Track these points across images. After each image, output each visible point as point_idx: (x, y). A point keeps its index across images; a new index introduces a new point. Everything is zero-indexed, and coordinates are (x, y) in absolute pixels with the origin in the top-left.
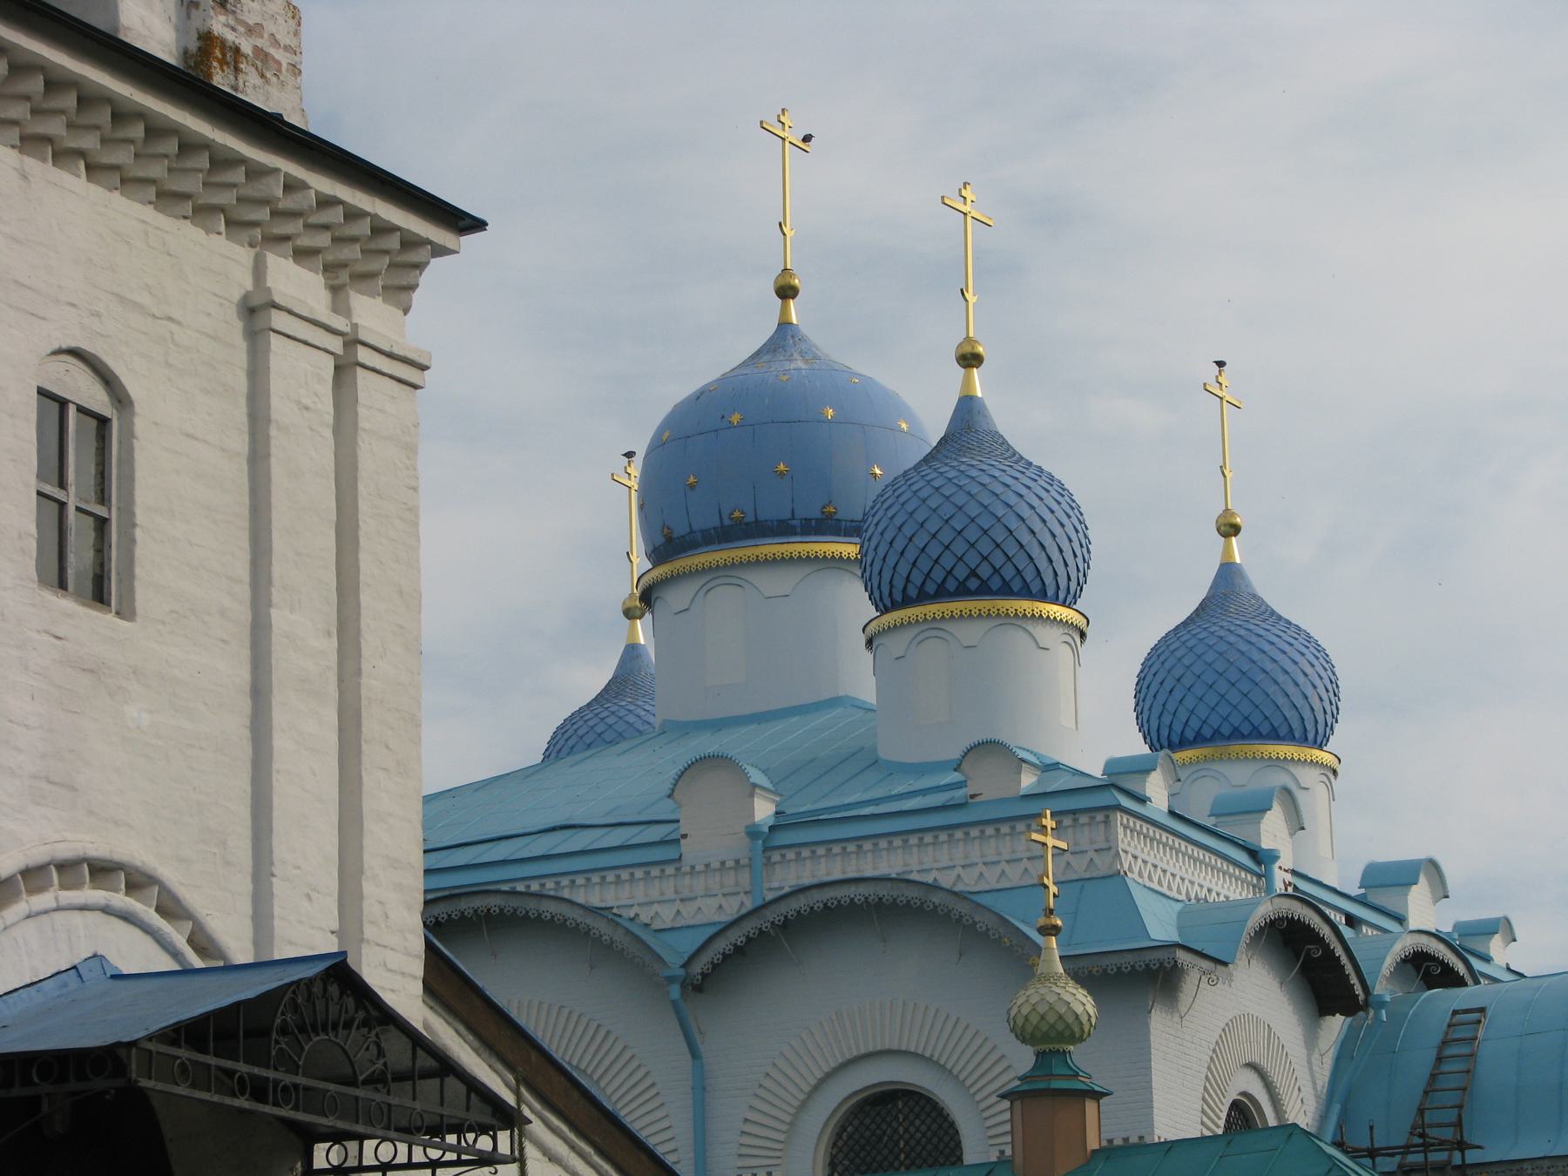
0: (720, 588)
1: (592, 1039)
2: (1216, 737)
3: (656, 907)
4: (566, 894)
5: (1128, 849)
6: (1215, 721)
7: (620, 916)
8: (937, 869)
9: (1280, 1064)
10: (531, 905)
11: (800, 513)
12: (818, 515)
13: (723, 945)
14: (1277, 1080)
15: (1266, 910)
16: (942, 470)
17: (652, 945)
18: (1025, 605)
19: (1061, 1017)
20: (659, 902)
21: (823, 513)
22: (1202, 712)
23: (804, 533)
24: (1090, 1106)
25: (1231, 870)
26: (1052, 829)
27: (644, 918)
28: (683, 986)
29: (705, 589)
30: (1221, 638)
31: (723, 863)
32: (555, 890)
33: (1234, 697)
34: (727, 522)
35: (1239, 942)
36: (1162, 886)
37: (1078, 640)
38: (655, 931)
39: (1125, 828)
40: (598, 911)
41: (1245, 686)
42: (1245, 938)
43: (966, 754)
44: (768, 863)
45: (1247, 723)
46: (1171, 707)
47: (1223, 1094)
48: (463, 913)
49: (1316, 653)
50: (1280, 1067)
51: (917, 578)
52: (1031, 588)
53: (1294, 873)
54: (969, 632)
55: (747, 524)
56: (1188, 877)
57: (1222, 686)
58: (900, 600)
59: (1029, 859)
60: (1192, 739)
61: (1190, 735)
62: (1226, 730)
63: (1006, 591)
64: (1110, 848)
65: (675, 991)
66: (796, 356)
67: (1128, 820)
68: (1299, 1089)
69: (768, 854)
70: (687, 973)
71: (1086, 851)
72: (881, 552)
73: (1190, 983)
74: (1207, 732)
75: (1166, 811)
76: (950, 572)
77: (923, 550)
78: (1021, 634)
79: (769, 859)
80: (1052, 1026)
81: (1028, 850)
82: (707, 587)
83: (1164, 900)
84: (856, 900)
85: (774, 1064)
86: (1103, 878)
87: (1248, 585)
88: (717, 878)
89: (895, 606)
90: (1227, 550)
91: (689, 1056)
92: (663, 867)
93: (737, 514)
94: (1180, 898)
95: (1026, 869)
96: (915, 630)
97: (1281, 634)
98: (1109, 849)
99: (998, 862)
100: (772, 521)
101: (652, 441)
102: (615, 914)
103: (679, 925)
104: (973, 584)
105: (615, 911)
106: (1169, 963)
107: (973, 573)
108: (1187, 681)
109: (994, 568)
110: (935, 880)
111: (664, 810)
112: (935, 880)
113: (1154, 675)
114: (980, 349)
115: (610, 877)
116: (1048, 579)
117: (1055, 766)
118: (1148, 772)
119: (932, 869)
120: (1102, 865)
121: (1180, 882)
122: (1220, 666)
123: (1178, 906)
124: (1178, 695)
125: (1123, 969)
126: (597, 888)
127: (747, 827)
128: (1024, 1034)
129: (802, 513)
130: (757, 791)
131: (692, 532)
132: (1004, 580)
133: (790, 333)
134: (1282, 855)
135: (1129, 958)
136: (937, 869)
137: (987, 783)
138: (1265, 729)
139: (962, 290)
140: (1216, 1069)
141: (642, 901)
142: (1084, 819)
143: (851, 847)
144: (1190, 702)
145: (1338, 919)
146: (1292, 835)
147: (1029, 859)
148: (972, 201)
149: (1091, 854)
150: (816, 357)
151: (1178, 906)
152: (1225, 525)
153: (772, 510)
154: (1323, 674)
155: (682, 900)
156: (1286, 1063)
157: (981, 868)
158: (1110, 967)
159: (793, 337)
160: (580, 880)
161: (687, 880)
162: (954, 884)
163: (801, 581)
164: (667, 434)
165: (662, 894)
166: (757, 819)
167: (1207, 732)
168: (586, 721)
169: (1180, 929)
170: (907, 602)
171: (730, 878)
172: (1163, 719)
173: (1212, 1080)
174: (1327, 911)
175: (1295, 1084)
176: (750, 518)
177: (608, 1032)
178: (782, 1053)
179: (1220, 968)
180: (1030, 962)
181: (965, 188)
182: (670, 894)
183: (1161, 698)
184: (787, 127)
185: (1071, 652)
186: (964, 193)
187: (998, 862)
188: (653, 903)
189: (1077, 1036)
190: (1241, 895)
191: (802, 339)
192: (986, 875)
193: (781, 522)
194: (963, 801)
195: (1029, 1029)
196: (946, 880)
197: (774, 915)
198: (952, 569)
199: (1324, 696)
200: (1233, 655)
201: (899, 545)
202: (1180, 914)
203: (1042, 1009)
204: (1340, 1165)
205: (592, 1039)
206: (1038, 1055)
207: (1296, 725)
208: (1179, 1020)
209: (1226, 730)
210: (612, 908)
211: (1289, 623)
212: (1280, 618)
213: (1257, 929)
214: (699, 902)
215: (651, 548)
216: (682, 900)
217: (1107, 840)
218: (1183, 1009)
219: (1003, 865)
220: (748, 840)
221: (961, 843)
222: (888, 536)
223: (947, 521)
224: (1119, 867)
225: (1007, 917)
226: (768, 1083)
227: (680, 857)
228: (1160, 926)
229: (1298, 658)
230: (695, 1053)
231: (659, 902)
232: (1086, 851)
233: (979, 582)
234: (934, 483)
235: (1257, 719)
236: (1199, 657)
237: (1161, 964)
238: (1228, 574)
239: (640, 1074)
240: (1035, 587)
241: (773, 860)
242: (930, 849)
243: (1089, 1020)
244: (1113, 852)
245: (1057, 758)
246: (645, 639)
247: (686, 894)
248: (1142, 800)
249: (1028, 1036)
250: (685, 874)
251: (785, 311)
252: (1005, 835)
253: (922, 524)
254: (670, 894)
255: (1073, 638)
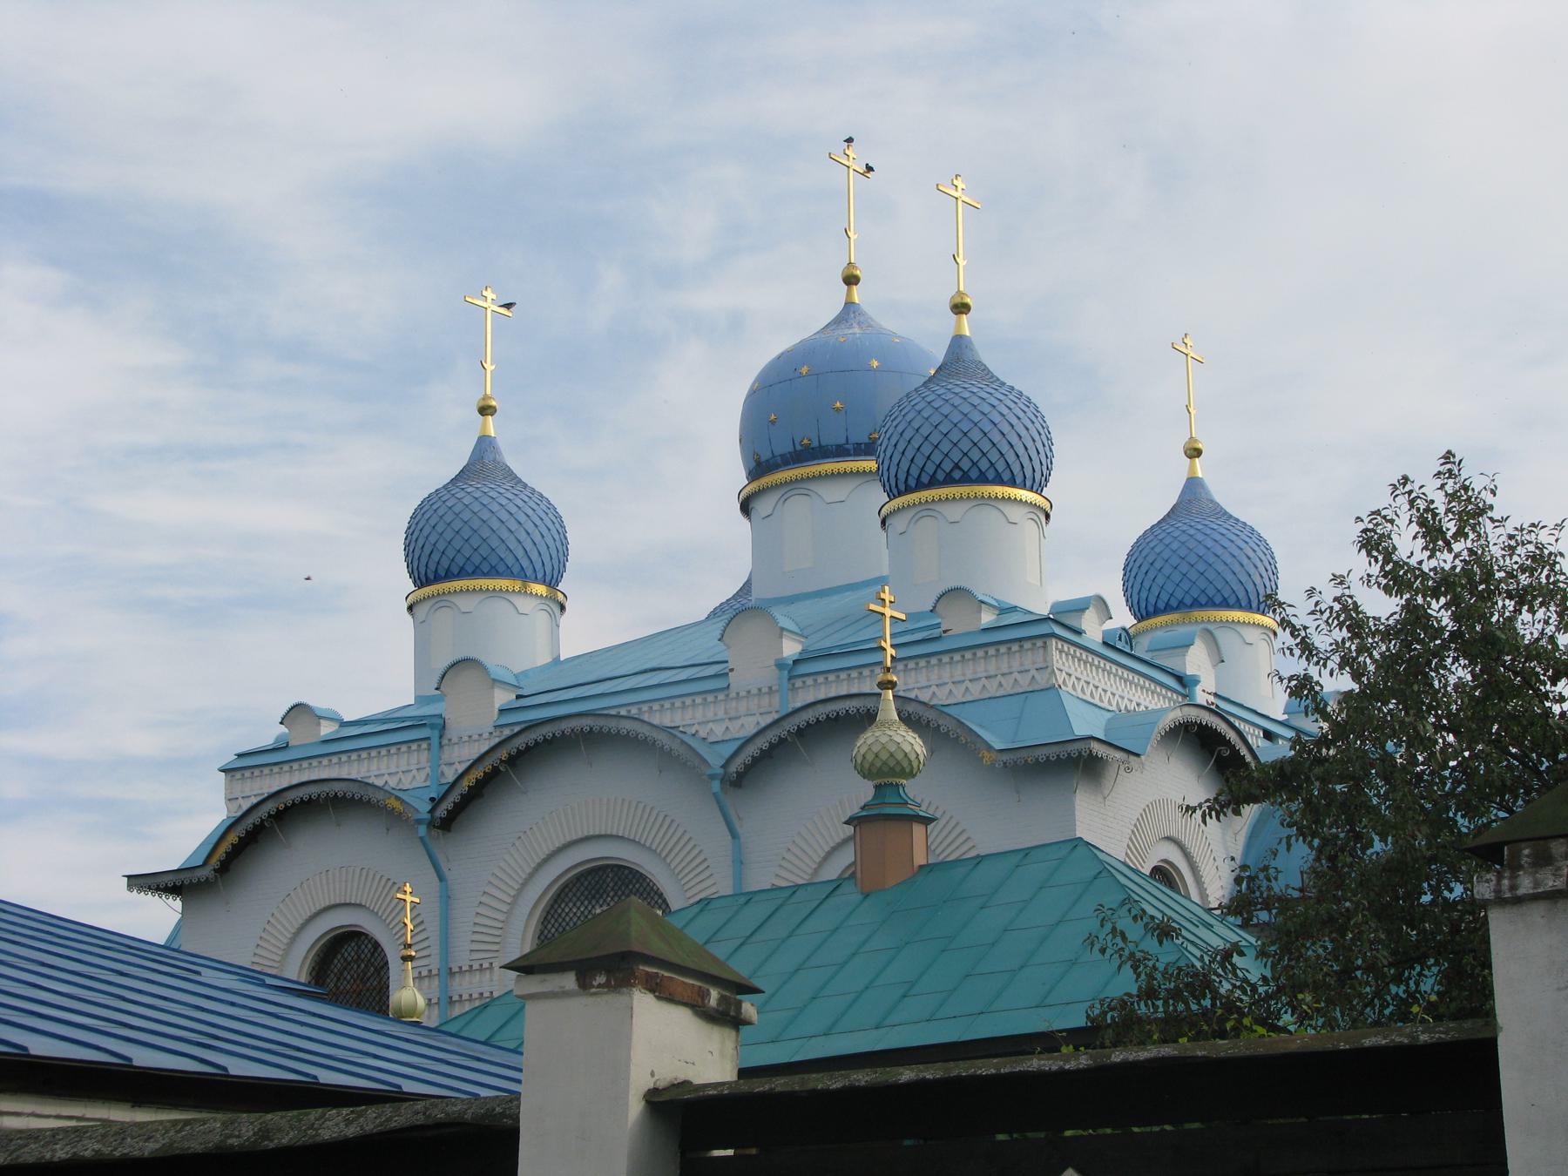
0: (797, 497)
1: (661, 826)
2: (1181, 606)
3: (711, 725)
4: (646, 717)
5: (1062, 668)
6: (1179, 595)
7: (685, 733)
8: (918, 688)
9: (1197, 839)
10: (612, 724)
11: (853, 439)
12: (867, 441)
13: (752, 750)
14: (1197, 855)
15: (1177, 715)
16: (939, 392)
17: (701, 753)
18: (999, 490)
19: (892, 755)
20: (713, 721)
21: (870, 438)
22: (1170, 588)
23: (855, 455)
24: (918, 830)
25: (1158, 690)
26: (891, 602)
27: (702, 734)
28: (722, 781)
29: (783, 499)
30: (1191, 536)
31: (760, 690)
32: (639, 714)
33: (1193, 575)
34: (798, 448)
35: (1149, 738)
36: (1094, 698)
37: (1272, 636)
38: (712, 743)
39: (1061, 652)
40: (669, 730)
41: (1201, 567)
42: (1155, 736)
43: (939, 599)
44: (794, 689)
45: (1203, 595)
46: (1147, 585)
47: (1143, 860)
48: (563, 732)
49: (1265, 550)
50: (1196, 842)
51: (915, 472)
52: (1229, 601)
53: (1216, 695)
54: (954, 512)
55: (813, 449)
56: (1119, 692)
57: (1184, 568)
58: (903, 489)
59: (986, 678)
60: (1163, 608)
61: (1161, 605)
62: (1188, 601)
63: (983, 479)
64: (1047, 667)
65: (716, 786)
66: (855, 325)
67: (1062, 646)
68: (1214, 859)
69: (792, 681)
70: (725, 772)
71: (1029, 670)
72: (895, 460)
73: (1111, 773)
74: (1174, 603)
75: (1101, 641)
76: (939, 466)
77: (918, 449)
78: (995, 513)
79: (793, 685)
80: (885, 763)
81: (986, 671)
82: (785, 497)
83: (1097, 710)
84: (850, 712)
85: (794, 842)
86: (1042, 690)
87: (1207, 492)
88: (756, 701)
89: (900, 494)
90: (1192, 468)
91: (730, 837)
92: (715, 694)
93: (805, 441)
94: (1111, 708)
95: (984, 686)
96: (912, 512)
97: (1231, 528)
98: (1046, 668)
99: (963, 681)
100: (832, 446)
101: (749, 392)
102: (681, 732)
103: (727, 738)
104: (957, 475)
105: (681, 729)
106: (1085, 752)
107: (957, 466)
108: (1158, 565)
109: (972, 461)
110: (916, 696)
111: (719, 652)
112: (916, 696)
113: (1139, 567)
114: (968, 300)
115: (678, 703)
116: (1016, 469)
117: (1014, 609)
118: (1083, 610)
119: (914, 688)
120: (1042, 680)
121: (1103, 693)
122: (1183, 553)
123: (1109, 715)
124: (1151, 575)
125: (1051, 758)
126: (668, 712)
127: (776, 660)
128: (866, 772)
129: (854, 439)
130: (785, 633)
131: (774, 456)
132: (980, 470)
133: (852, 309)
134: (1202, 680)
135: (1055, 749)
136: (918, 688)
137: (957, 622)
138: (1218, 599)
139: (954, 256)
140: (1137, 840)
141: (700, 721)
142: (1027, 645)
143: (854, 674)
144: (1160, 580)
145: (1247, 729)
146: (1214, 666)
147: (986, 678)
148: (963, 189)
149: (1033, 672)
150: (870, 326)
151: (1109, 715)
152: (1190, 449)
153: (832, 438)
154: (1263, 558)
155: (730, 719)
156: (1198, 832)
157: (950, 686)
158: (1041, 757)
159: (854, 313)
160: (656, 706)
161: (734, 704)
162: (931, 699)
163: (853, 490)
164: (757, 385)
165: (715, 715)
166: (785, 655)
167: (1174, 603)
168: (444, 502)
169: (1107, 731)
170: (909, 490)
171: (765, 700)
172: (1141, 594)
173: (1133, 848)
174: (1232, 720)
175: (1208, 849)
176: (815, 444)
177: (672, 821)
178: (799, 833)
179: (1132, 758)
180: (980, 755)
181: (956, 179)
182: (721, 714)
183: (1139, 580)
184: (851, 159)
185: (1036, 526)
186: (955, 182)
187: (963, 681)
188: (708, 722)
189: (907, 770)
190: (1156, 704)
191: (862, 314)
192: (971, 689)
193: (839, 446)
194: (938, 636)
195: (867, 765)
196: (925, 696)
197: (791, 725)
198: (941, 463)
199: (1264, 574)
200: (1192, 544)
201: (901, 447)
202: (1109, 720)
203: (875, 749)
204: (1113, 871)
205: (661, 826)
206: (877, 787)
207: (1241, 595)
208: (1102, 800)
209: (1188, 601)
210: (679, 727)
211: (1238, 520)
212: (1231, 516)
213: (1167, 730)
214: (743, 720)
215: (748, 471)
216: (730, 719)
217: (1045, 661)
218: (1106, 792)
219: (968, 684)
220: (777, 671)
221: (936, 668)
222: (893, 441)
223: (936, 427)
224: (1054, 681)
225: (963, 720)
226: (788, 856)
227: (729, 685)
228: (1085, 723)
229: (1243, 545)
230: (734, 834)
231: (713, 721)
232: (1029, 670)
233: (961, 473)
234: (934, 404)
235: (1211, 592)
236: (1167, 546)
237: (1080, 753)
238: (1193, 486)
239: (696, 851)
240: (1006, 477)
241: (797, 686)
242: (913, 673)
243: (917, 757)
244: (1049, 670)
245: (1014, 603)
246: (495, 431)
247: (733, 714)
248: (1079, 632)
249: (866, 773)
250: (732, 699)
251: (849, 294)
252: (969, 660)
253: (927, 437)
254: (721, 714)
255: (1038, 516)
